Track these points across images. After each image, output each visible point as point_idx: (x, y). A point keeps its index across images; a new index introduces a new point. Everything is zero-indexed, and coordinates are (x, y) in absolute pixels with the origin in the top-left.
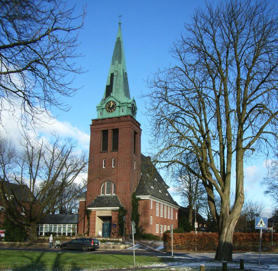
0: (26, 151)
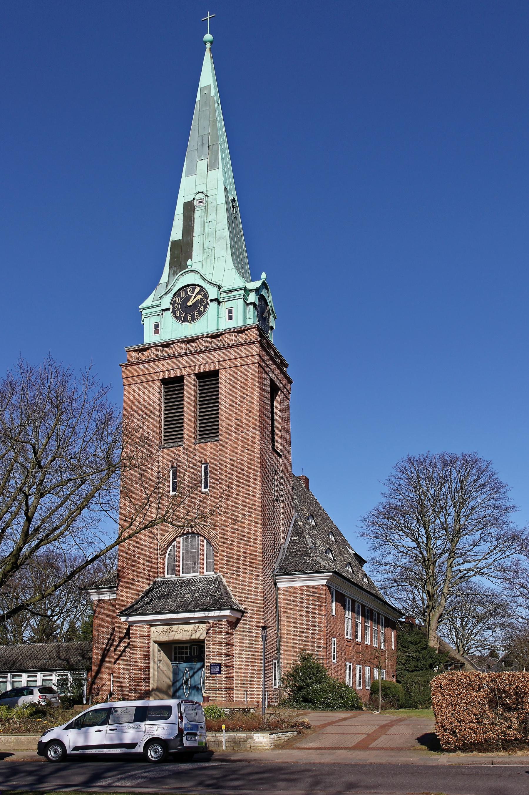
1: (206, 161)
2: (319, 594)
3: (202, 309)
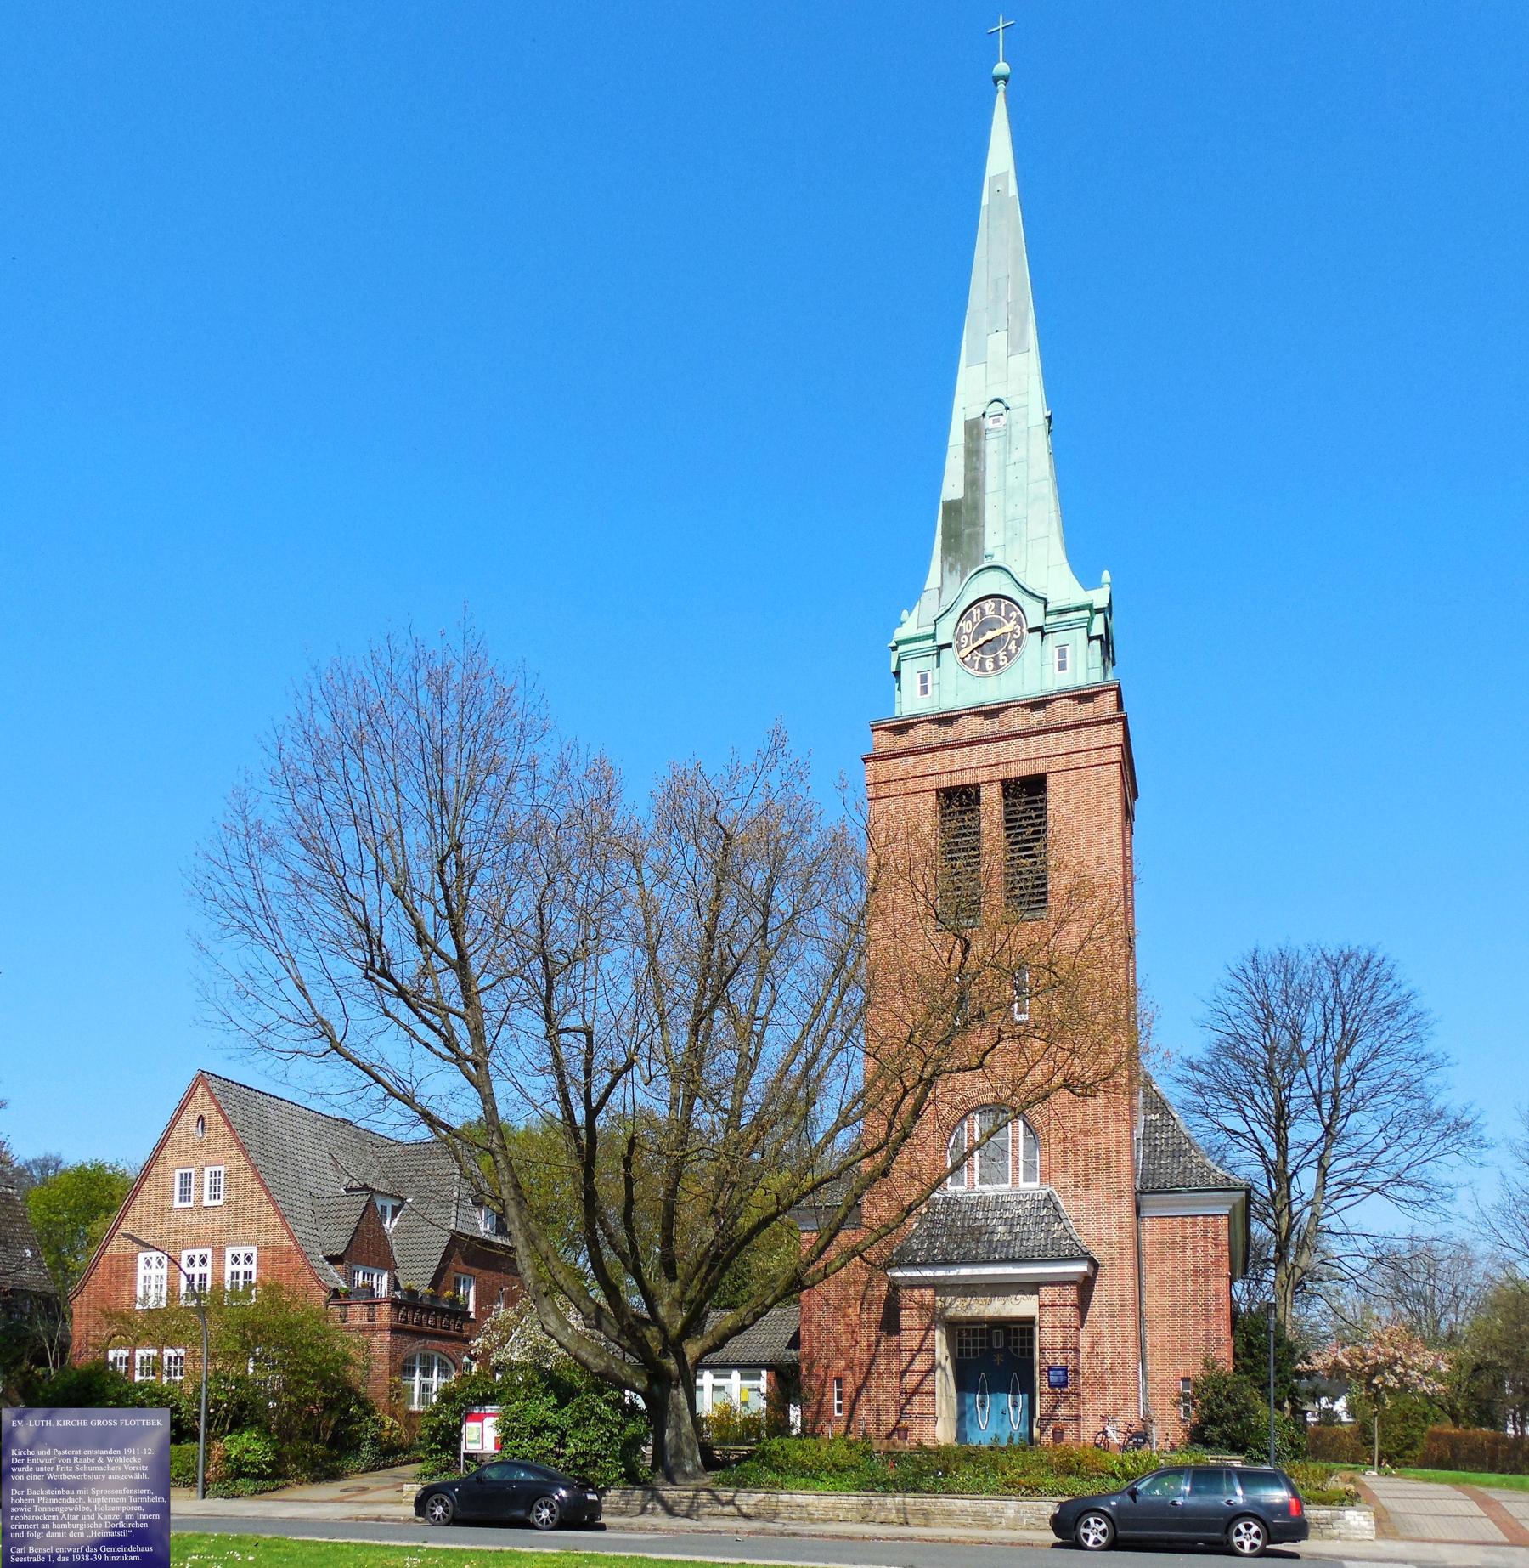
0: (549, 1119)
1: (1003, 335)
2: (1217, 1234)
3: (1012, 647)
